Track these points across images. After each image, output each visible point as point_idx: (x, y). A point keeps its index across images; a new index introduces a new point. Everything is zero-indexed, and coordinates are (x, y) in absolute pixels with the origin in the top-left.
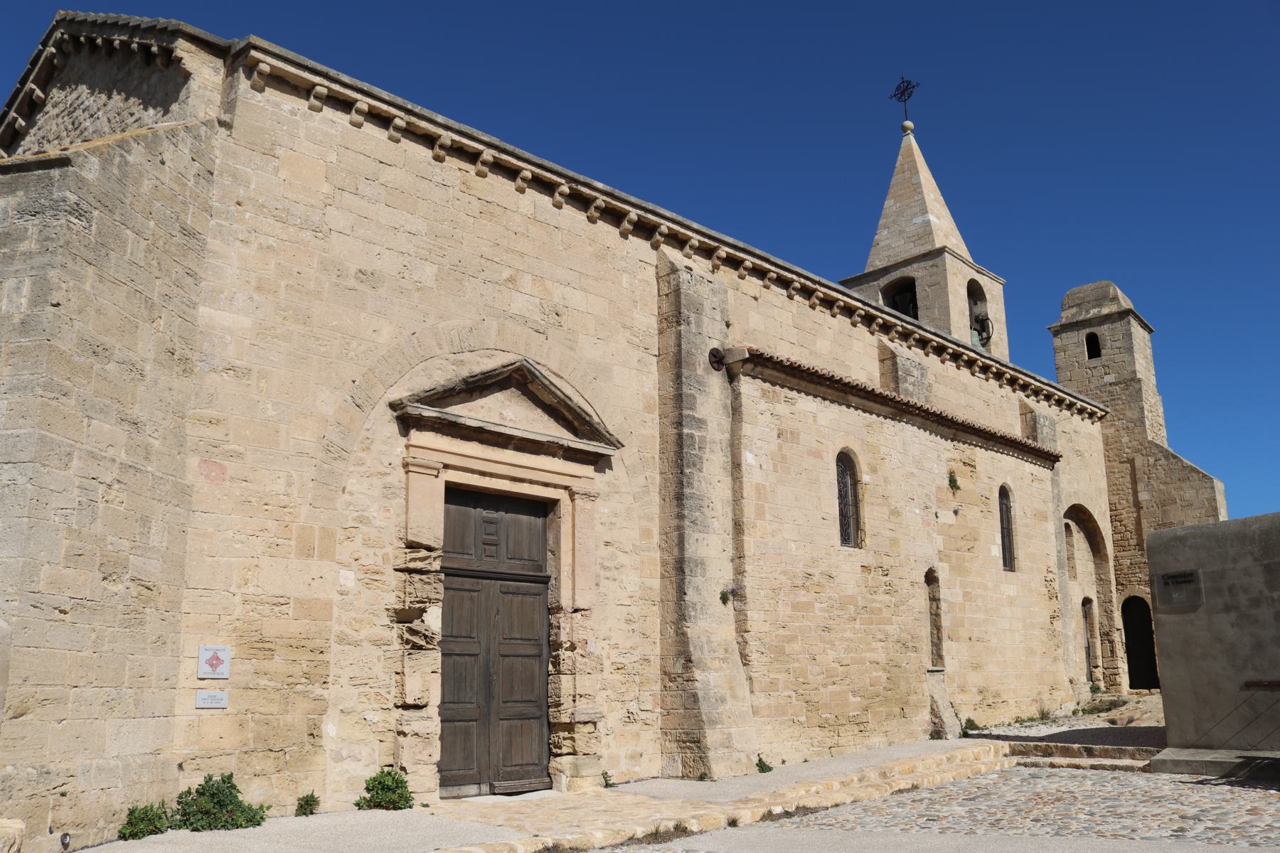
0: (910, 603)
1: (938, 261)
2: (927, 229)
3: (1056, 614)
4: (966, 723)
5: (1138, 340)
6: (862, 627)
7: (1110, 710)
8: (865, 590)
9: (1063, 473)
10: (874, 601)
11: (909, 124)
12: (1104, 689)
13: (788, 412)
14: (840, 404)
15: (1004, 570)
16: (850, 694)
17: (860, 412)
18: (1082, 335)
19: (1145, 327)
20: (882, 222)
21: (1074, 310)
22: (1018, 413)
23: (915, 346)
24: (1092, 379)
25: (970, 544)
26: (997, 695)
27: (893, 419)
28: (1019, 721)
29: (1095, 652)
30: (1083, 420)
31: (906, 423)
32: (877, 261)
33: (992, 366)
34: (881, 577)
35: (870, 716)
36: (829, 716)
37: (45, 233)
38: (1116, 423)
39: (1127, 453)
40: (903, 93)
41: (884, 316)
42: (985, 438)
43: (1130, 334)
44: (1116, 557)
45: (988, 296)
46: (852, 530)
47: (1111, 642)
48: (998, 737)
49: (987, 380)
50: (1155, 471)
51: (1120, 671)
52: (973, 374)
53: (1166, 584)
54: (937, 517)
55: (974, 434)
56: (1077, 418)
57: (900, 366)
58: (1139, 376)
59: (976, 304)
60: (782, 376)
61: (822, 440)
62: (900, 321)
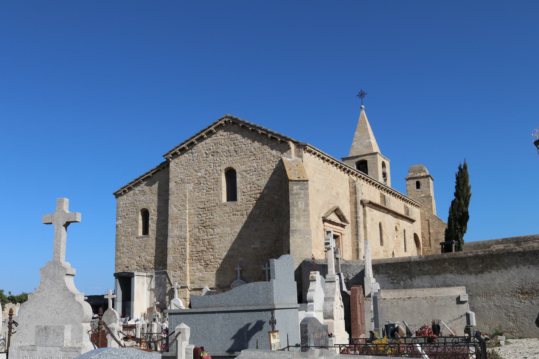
2: (370, 144)
19: (433, 180)
20: (354, 139)
21: (412, 173)
32: (353, 153)
37: (305, 194)
44: (423, 248)
45: (386, 166)
55: (400, 216)
58: (431, 195)
62: (360, 173)
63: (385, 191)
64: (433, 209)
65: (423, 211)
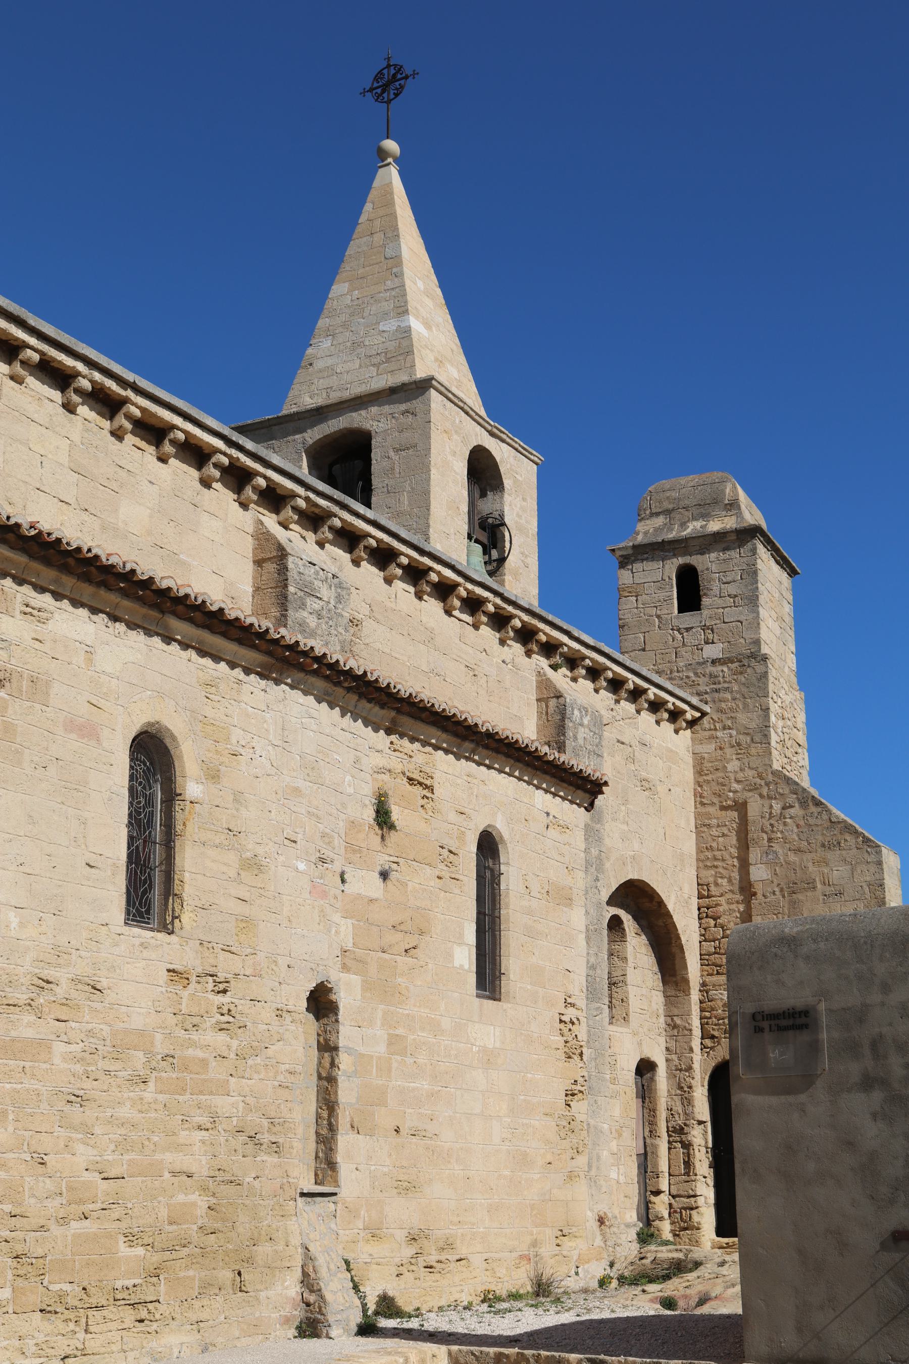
0: (270, 1052)
1: (416, 404)
2: (405, 343)
3: (579, 1088)
4: (378, 1304)
5: (768, 585)
6: (160, 1097)
7: (667, 1278)
8: (173, 1020)
9: (614, 820)
10: (193, 1044)
11: (391, 145)
12: (670, 1237)
13: (27, 637)
14: (149, 633)
15: (478, 996)
16: (122, 1239)
17: (192, 653)
18: (670, 568)
19: (783, 562)
20: (322, 323)
21: (660, 521)
22: (534, 697)
23: (332, 543)
24: (682, 651)
25: (411, 941)
26: (448, 1245)
27: (262, 676)
28: (489, 1299)
29: (656, 1165)
30: (658, 722)
31: (292, 687)
33: (487, 600)
34: (211, 996)
35: (162, 1288)
36: (67, 1287)
38: (719, 734)
39: (735, 792)
40: (385, 87)
41: (270, 473)
42: (456, 735)
43: (756, 572)
44: (704, 984)
45: (507, 482)
46: (156, 894)
47: (687, 1146)
48: (433, 1337)
49: (476, 627)
50: (781, 828)
51: (701, 1201)
52: (448, 613)
53: (759, 1030)
54: (343, 881)
56: (647, 718)
57: (292, 574)
58: (765, 650)
59: (483, 495)
60: (21, 559)
61: (102, 703)
63: (678, 725)
64: (774, 738)
65: (709, 748)
